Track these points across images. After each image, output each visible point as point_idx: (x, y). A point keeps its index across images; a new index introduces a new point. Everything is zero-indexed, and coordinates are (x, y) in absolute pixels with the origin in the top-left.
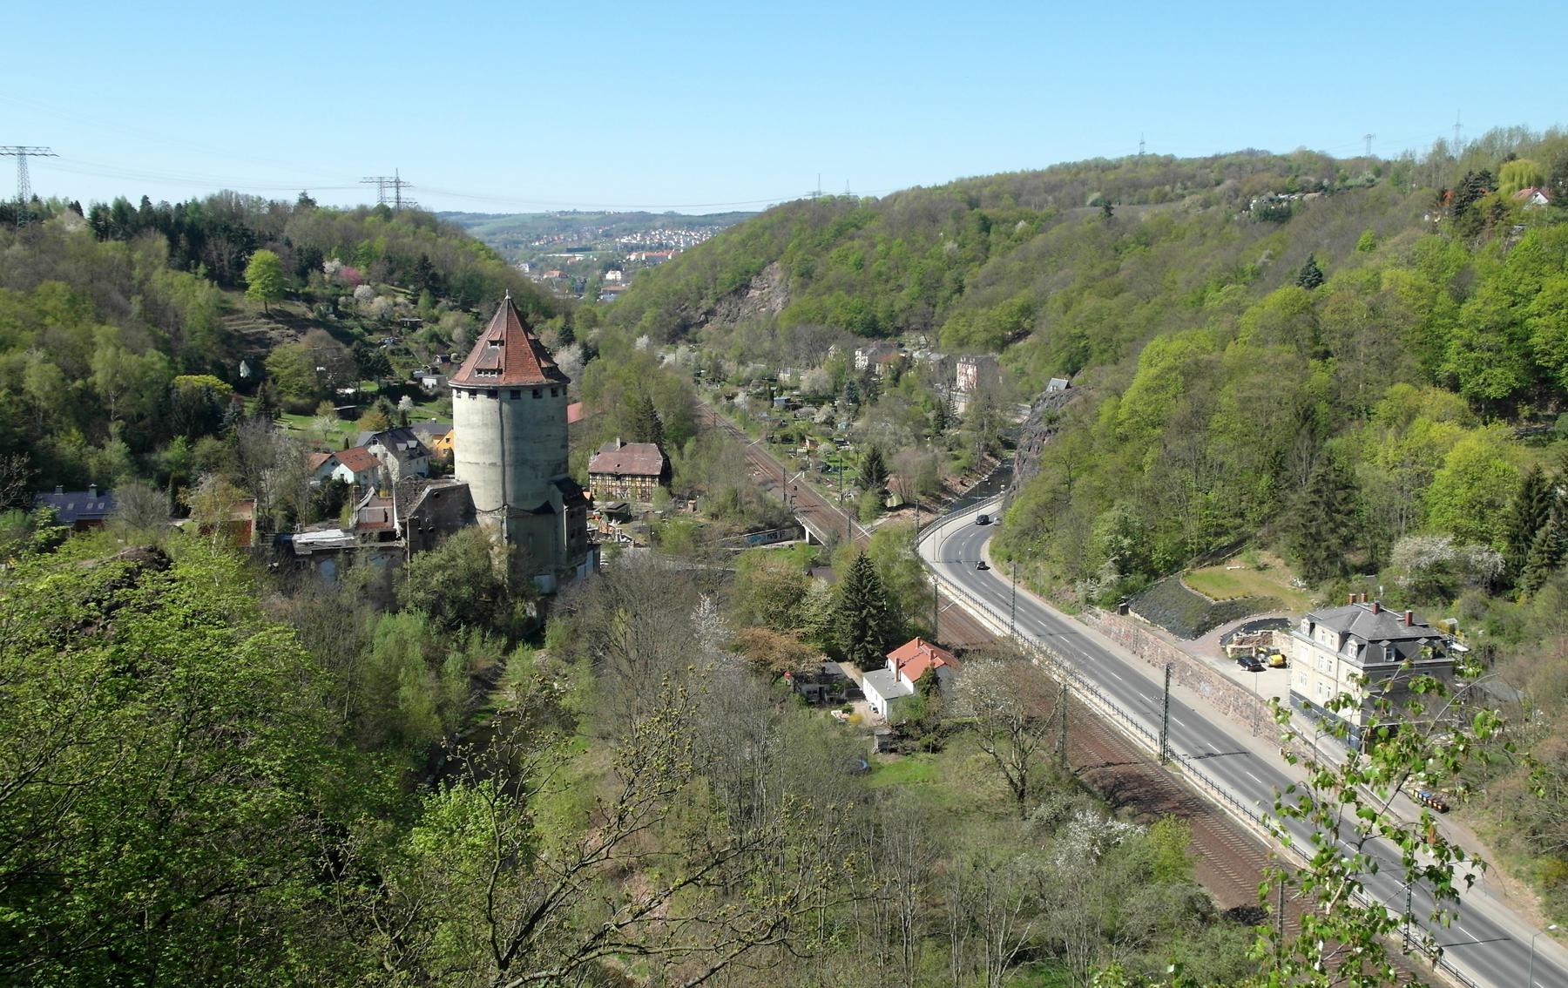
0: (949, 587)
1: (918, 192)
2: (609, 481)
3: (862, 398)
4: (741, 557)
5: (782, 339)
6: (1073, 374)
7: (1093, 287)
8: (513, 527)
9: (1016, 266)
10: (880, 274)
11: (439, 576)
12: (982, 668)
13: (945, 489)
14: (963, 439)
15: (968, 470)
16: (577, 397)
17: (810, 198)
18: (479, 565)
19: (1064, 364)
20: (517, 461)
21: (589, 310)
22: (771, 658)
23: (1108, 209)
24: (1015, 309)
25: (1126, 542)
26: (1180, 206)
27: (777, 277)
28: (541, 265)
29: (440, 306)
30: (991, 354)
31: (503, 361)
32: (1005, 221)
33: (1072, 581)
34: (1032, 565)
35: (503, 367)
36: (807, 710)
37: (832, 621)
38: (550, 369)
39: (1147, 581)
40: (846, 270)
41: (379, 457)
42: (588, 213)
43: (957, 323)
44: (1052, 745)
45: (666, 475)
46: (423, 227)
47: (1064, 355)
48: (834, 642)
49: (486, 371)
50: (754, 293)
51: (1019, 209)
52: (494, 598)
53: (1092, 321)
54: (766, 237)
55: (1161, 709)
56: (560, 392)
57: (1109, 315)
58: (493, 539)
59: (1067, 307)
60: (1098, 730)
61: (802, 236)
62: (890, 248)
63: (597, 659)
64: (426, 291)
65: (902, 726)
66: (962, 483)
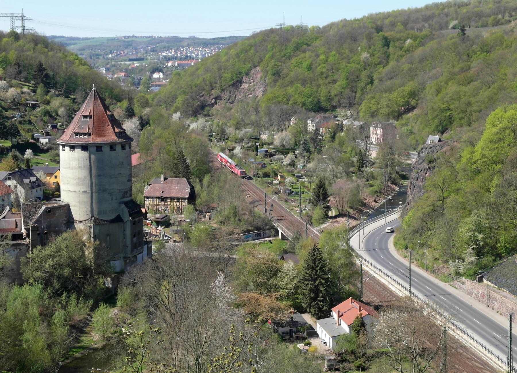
0: (369, 265)
1: (345, 23)
2: (157, 202)
3: (312, 149)
4: (240, 248)
5: (262, 114)
6: (442, 133)
7: (454, 79)
8: (97, 231)
9: (406, 67)
10: (322, 73)
11: (50, 262)
12: (392, 316)
13: (365, 205)
14: (375, 174)
15: (379, 193)
16: (137, 150)
17: (278, 27)
18: (76, 254)
19: (437, 127)
20: (100, 189)
21: (143, 97)
22: (260, 312)
23: (463, 30)
24: (405, 93)
25: (480, 236)
26: (508, 27)
27: (259, 76)
28: (113, 69)
29: (50, 94)
30: (391, 121)
31: (91, 128)
32: (398, 40)
33: (447, 261)
34: (421, 252)
35: (91, 131)
36: (284, 344)
37: (297, 288)
38: (120, 133)
39: (494, 261)
40: (302, 71)
41: (12, 187)
42: (142, 37)
43: (370, 102)
44: (438, 366)
45: (192, 198)
46: (39, 45)
47: (437, 121)
48: (299, 301)
49: (81, 134)
50: (245, 86)
51: (407, 32)
52: (85, 275)
53: (454, 99)
54: (252, 51)
55: (507, 343)
56: (127, 147)
57: (465, 96)
58: (85, 238)
59: (438, 91)
60: (467, 356)
61: (274, 51)
62: (328, 58)
63: (150, 313)
64: (41, 85)
65: (342, 354)
66: (375, 201)
